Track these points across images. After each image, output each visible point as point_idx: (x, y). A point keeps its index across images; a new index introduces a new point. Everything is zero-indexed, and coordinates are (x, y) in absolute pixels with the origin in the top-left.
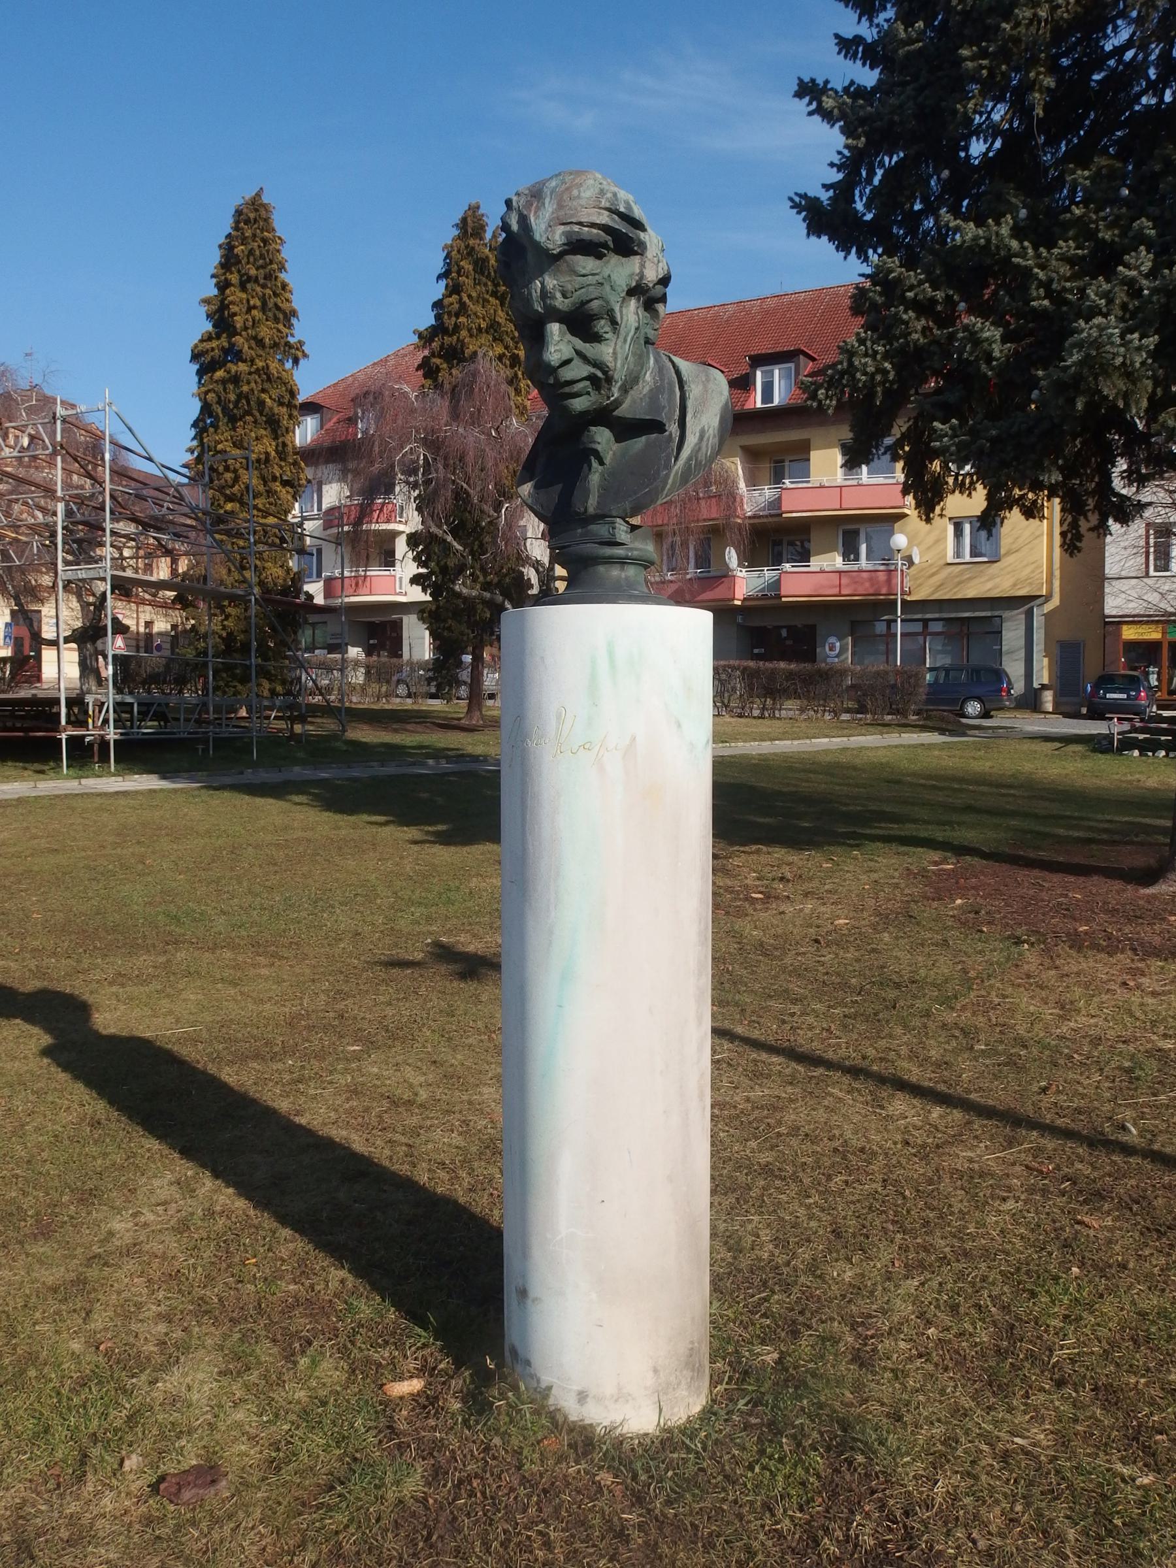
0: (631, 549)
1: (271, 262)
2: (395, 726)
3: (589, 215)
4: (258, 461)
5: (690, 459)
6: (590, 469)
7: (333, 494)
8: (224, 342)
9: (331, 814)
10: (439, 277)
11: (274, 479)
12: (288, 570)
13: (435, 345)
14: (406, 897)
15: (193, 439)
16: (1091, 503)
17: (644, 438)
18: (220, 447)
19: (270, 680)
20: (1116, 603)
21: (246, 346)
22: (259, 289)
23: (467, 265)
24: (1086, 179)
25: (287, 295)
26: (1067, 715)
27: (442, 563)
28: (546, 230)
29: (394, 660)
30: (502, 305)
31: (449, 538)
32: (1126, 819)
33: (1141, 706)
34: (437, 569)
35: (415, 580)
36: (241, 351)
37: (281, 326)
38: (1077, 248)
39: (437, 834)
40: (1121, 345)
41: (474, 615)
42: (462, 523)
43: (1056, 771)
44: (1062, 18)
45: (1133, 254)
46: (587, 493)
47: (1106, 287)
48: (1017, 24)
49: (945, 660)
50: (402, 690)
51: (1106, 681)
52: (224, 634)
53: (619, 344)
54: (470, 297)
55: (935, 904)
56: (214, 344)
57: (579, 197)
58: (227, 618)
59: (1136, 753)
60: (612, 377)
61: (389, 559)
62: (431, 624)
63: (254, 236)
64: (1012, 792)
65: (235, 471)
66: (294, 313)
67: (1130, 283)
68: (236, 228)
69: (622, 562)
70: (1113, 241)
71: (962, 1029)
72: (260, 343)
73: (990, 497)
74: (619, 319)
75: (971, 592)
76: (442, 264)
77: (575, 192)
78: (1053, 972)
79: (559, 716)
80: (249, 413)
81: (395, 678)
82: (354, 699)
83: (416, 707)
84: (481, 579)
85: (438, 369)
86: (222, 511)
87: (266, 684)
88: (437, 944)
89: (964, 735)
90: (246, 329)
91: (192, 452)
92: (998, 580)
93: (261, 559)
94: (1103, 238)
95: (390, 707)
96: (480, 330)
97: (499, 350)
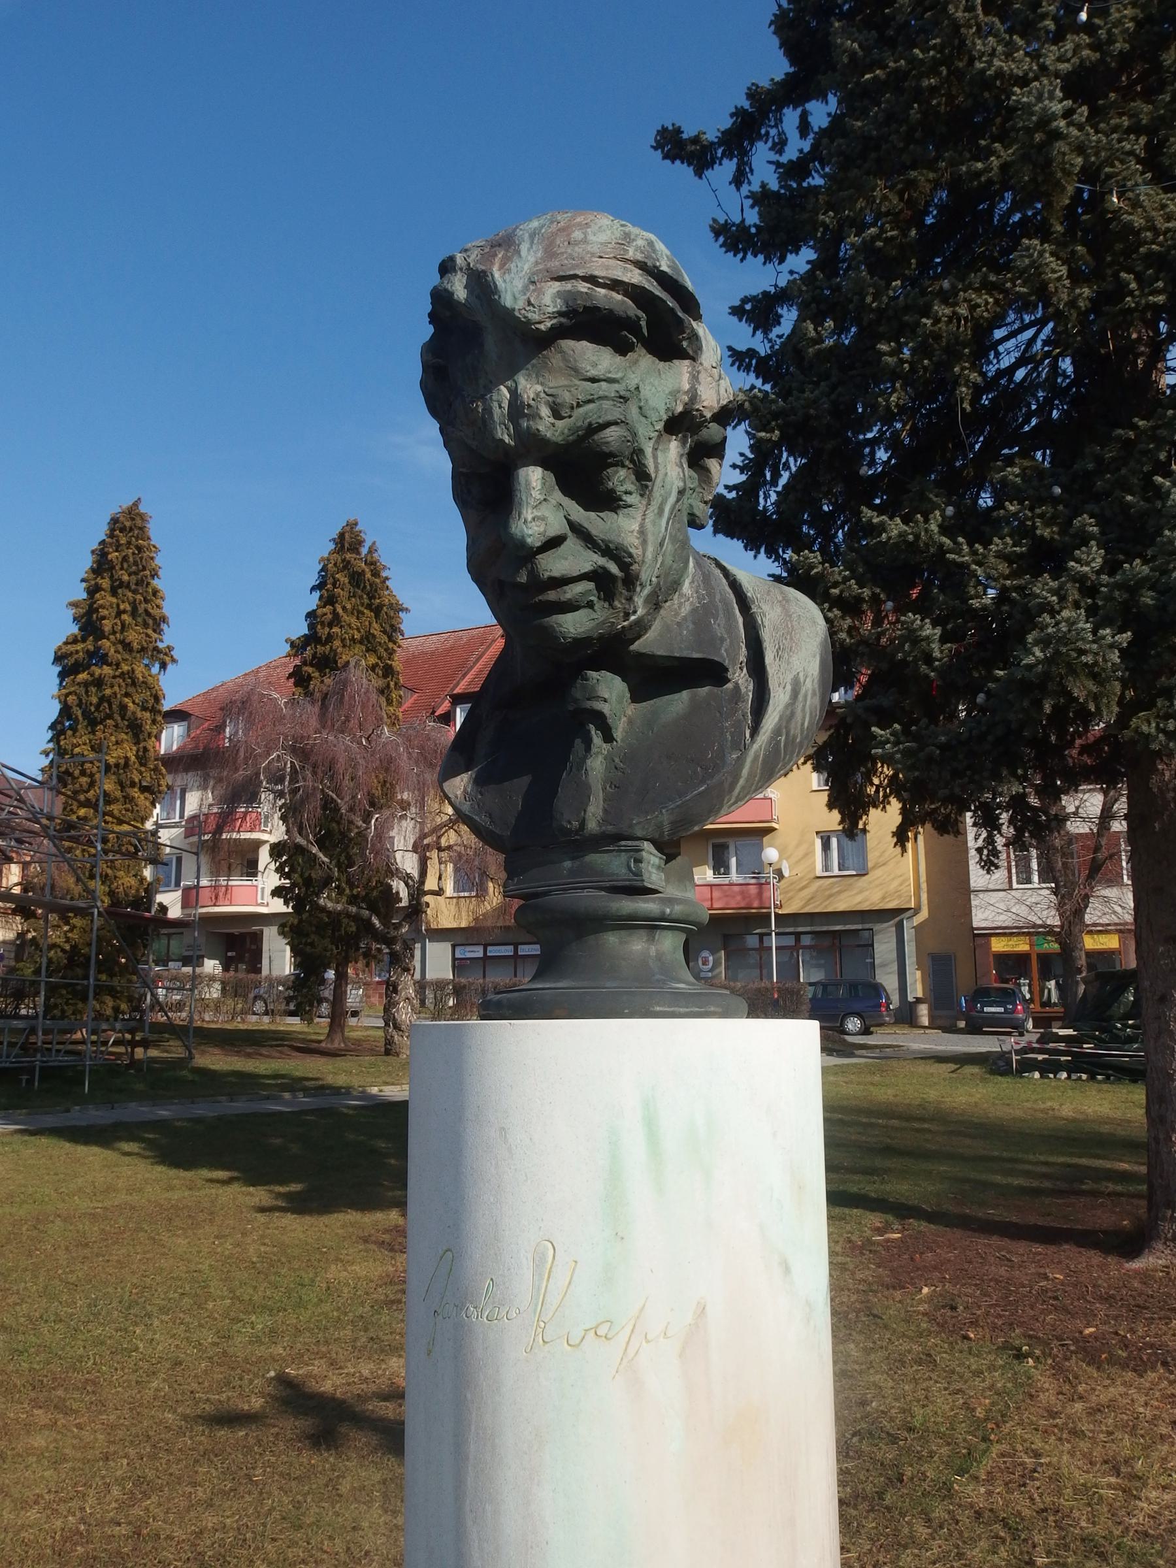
0: (670, 901)
1: (144, 569)
2: (249, 1050)
3: (607, 268)
4: (117, 765)
5: (777, 732)
6: (588, 749)
7: (194, 802)
8: (89, 645)
9: (164, 1169)
10: (313, 589)
11: (133, 785)
12: (143, 879)
13: (309, 652)
14: (246, 1297)
15: (49, 741)
16: (1004, 817)
17: (685, 694)
18: (77, 750)
19: (114, 997)
20: (981, 917)
21: (112, 650)
22: (130, 594)
23: (342, 578)
24: (1017, 476)
25: (159, 601)
26: (946, 1030)
27: (307, 875)
28: (525, 289)
29: (252, 976)
30: (377, 617)
31: (315, 850)
32: (1061, 1159)
33: (1018, 1019)
34: (300, 880)
35: (277, 892)
36: (106, 655)
37: (150, 631)
38: (1014, 545)
39: (288, 1196)
40: (1094, 642)
41: (339, 930)
42: (329, 833)
43: (963, 1099)
44: (982, 317)
45: (1084, 549)
46: (583, 793)
47: (1054, 584)
48: (937, 321)
49: (818, 976)
50: (259, 1006)
51: (981, 994)
52: (67, 947)
53: (651, 515)
54: (344, 608)
55: (898, 1295)
56: (79, 647)
57: (585, 241)
58: (71, 930)
59: (1037, 1075)
60: (637, 577)
61: (251, 869)
62: (292, 939)
63: (129, 543)
64: (926, 1126)
65: (92, 775)
66: (164, 619)
67: (1081, 579)
68: (111, 536)
69: (652, 925)
70: (1052, 538)
71: (1004, 1523)
72: (127, 646)
73: (904, 811)
74: (651, 469)
75: (841, 905)
76: (317, 576)
77: (577, 235)
78: (1079, 1406)
79: (539, 1261)
80: (110, 717)
81: (251, 995)
82: (207, 1018)
83: (273, 1027)
84: (348, 891)
85: (310, 678)
86: (74, 817)
87: (110, 1002)
88: (283, 1380)
89: (851, 1055)
90: (114, 633)
91: (47, 755)
92: (867, 893)
93: (112, 867)
94: (1042, 536)
95: (245, 1027)
96: (353, 639)
97: (372, 660)
